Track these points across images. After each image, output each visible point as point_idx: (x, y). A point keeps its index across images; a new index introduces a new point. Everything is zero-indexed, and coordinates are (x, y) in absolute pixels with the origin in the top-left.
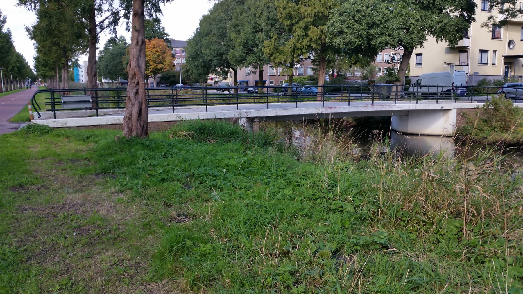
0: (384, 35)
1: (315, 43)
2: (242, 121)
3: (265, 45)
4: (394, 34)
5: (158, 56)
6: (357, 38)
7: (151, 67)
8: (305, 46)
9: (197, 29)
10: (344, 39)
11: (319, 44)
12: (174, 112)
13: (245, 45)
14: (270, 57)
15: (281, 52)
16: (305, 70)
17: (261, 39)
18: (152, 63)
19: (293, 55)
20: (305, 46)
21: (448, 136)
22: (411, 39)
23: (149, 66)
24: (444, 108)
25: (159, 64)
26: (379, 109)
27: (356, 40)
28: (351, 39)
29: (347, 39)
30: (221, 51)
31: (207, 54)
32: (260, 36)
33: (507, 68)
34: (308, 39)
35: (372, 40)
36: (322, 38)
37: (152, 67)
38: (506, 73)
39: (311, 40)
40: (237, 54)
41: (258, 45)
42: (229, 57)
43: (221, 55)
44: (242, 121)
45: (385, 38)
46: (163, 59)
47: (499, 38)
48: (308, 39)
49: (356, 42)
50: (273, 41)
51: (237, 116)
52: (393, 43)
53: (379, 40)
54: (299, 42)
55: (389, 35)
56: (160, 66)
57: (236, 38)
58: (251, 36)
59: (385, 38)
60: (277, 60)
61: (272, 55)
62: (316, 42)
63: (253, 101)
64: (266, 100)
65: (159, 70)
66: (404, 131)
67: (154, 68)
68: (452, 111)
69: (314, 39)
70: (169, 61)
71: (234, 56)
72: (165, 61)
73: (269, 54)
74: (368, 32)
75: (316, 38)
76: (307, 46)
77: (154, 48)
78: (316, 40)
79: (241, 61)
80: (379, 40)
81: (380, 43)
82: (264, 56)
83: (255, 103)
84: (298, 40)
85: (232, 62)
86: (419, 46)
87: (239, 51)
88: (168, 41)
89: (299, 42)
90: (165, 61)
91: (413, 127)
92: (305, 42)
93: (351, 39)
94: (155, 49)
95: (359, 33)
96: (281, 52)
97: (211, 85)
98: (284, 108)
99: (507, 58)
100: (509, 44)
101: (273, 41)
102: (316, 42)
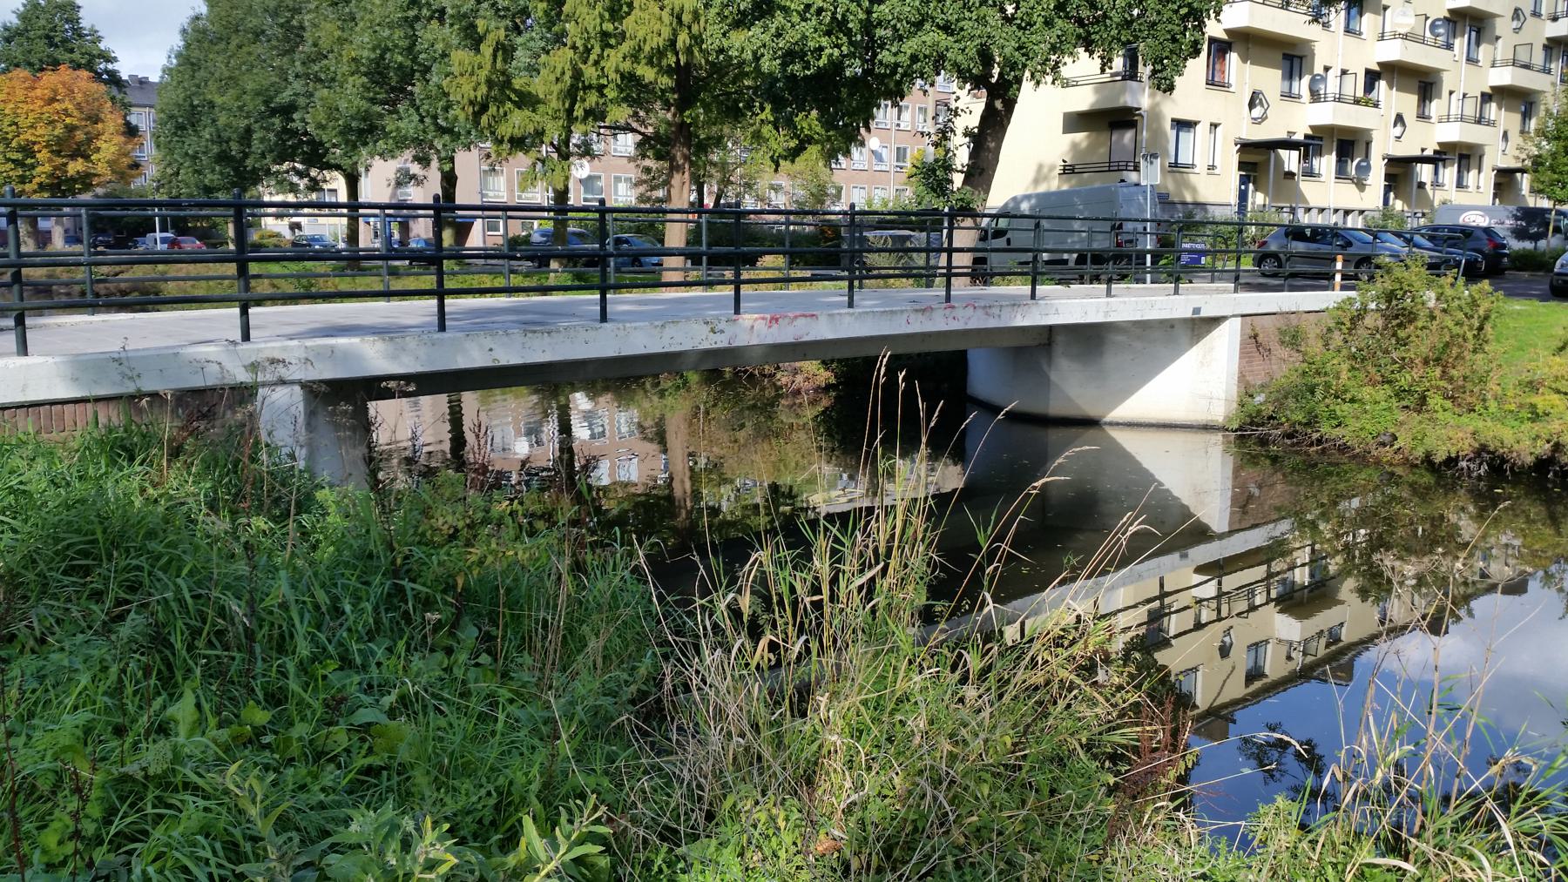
0: (927, 26)
1: (650, 63)
2: (281, 408)
3: (455, 69)
4: (966, 24)
5: (71, 129)
6: (828, 33)
7: (39, 169)
8: (612, 76)
9: (197, 18)
10: (778, 35)
11: (669, 71)
12: (23, 349)
13: (377, 72)
14: (477, 116)
15: (527, 101)
16: (612, 172)
17: (439, 46)
18: (43, 155)
19: (570, 111)
20: (612, 76)
21: (1207, 428)
22: (1019, 48)
23: (33, 167)
24: (1204, 314)
25: (73, 157)
26: (973, 324)
27: (824, 41)
28: (804, 37)
29: (792, 36)
30: (285, 97)
31: (229, 110)
32: (433, 35)
33: (1244, 180)
34: (626, 47)
35: (882, 47)
36: (680, 44)
37: (48, 168)
38: (1243, 196)
39: (635, 56)
40: (343, 105)
41: (428, 69)
42: (309, 121)
43: (287, 111)
44: (281, 408)
45: (931, 37)
46: (89, 140)
47: (1223, 86)
48: (626, 47)
49: (821, 49)
50: (487, 49)
51: (243, 376)
52: (960, 58)
53: (910, 46)
54: (593, 57)
55: (947, 28)
56: (75, 167)
57: (341, 41)
58: (399, 33)
59: (931, 37)
60: (505, 130)
61: (484, 108)
62: (655, 58)
63: (379, 287)
64: (429, 281)
65: (73, 180)
66: (1033, 406)
67: (51, 176)
68: (1225, 326)
69: (647, 48)
70: (113, 149)
71: (332, 111)
72: (98, 150)
73: (471, 103)
74: (869, 12)
75: (655, 42)
76: (623, 76)
77: (52, 100)
78: (660, 53)
79: (364, 133)
80: (910, 46)
81: (914, 58)
82: (455, 111)
83: (388, 294)
84: (588, 51)
85: (329, 137)
86: (1049, 79)
87: (351, 96)
88: (114, 80)
89: (593, 57)
90: (98, 150)
91: (1071, 388)
92: (615, 60)
93: (804, 37)
94: (57, 106)
95: (834, 13)
96: (527, 101)
97: (278, 235)
98: (534, 324)
99: (1246, 147)
100: (1252, 105)
101: (487, 49)
102: (655, 58)
